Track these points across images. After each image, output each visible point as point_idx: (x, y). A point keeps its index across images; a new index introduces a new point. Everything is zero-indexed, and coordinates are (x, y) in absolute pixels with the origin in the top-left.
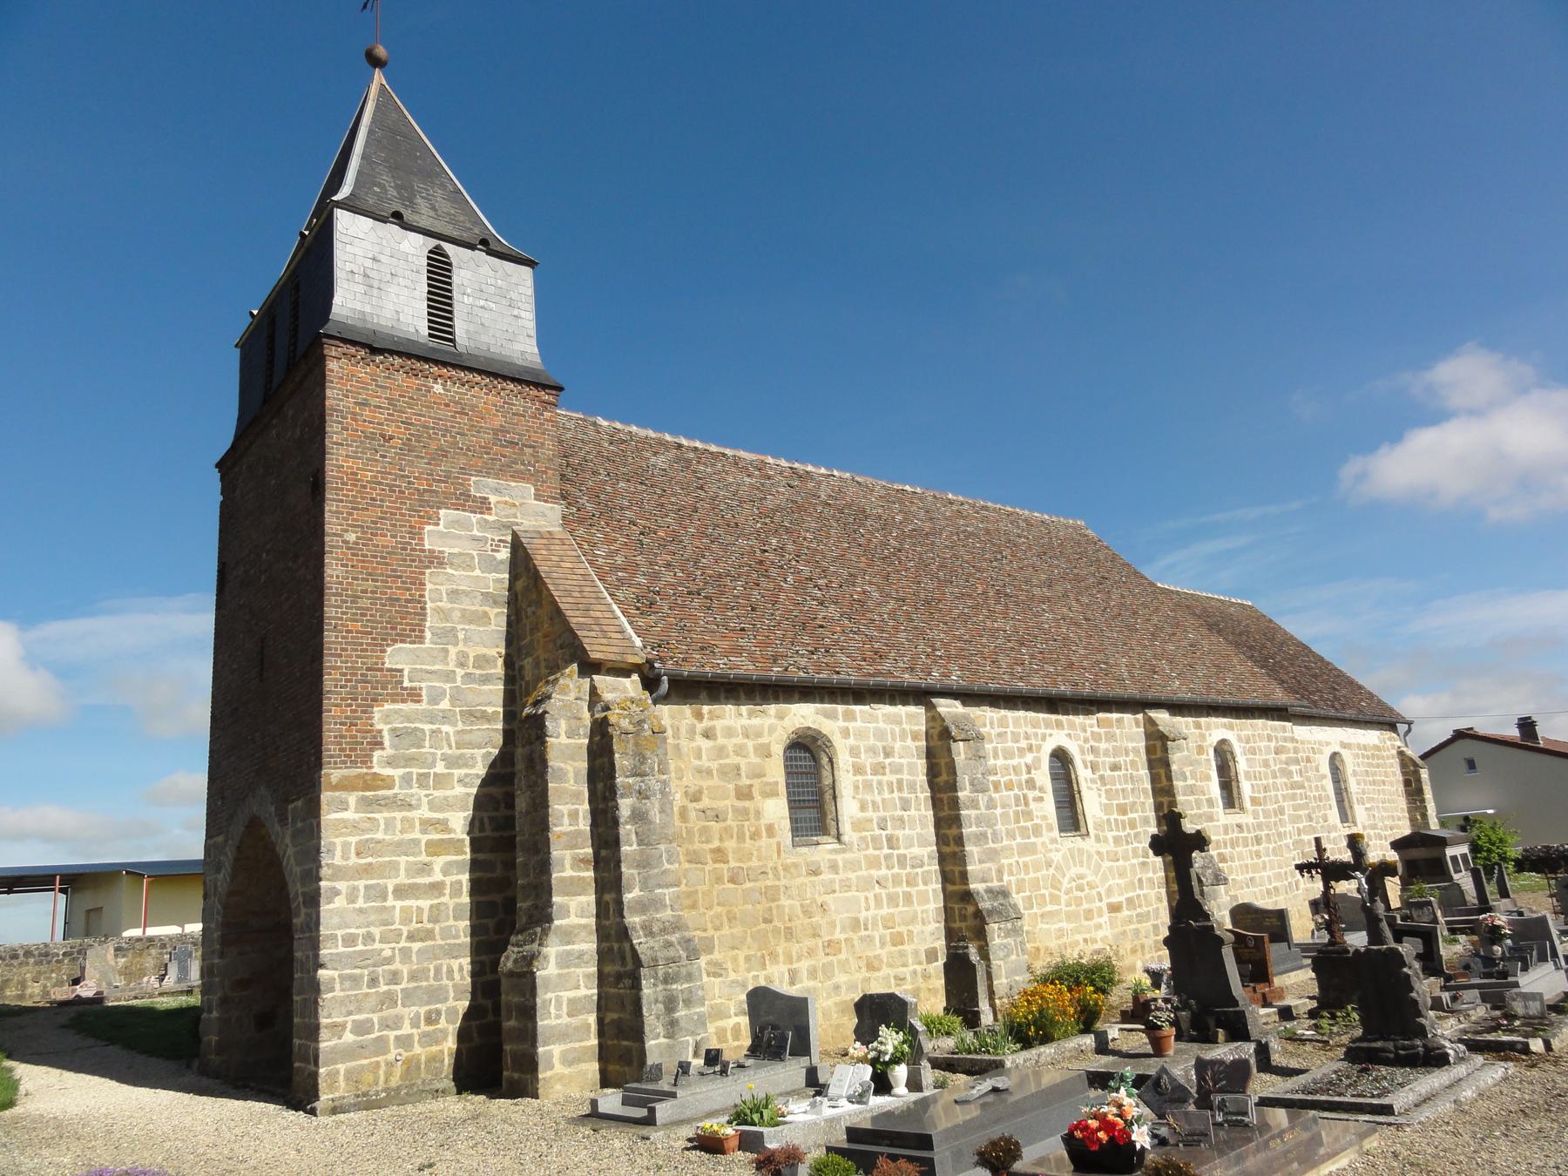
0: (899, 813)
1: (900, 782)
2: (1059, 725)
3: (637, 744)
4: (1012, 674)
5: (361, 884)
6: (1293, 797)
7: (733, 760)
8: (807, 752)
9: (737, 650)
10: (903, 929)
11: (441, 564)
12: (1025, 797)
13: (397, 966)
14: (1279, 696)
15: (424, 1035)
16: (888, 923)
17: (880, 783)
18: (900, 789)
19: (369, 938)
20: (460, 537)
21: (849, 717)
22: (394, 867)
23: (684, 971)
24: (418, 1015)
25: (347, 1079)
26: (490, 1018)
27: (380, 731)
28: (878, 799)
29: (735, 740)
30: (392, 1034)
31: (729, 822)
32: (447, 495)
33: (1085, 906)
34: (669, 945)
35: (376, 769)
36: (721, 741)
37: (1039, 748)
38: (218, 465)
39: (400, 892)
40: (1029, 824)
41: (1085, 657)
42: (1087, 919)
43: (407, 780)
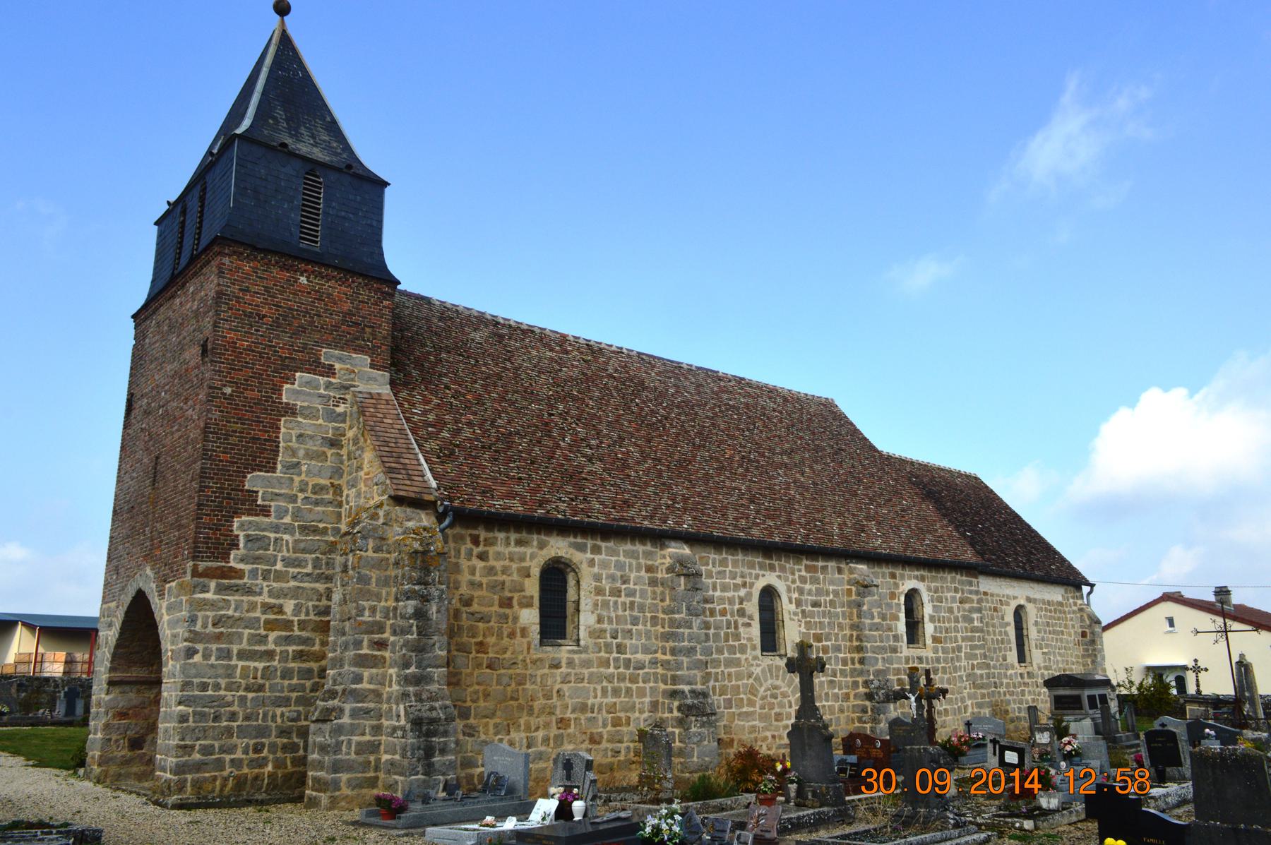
0: (629, 627)
1: (632, 603)
2: (772, 568)
3: (423, 561)
4: (736, 526)
5: (214, 647)
6: (971, 639)
7: (501, 578)
8: (555, 578)
9: (511, 495)
10: (622, 715)
11: (294, 414)
12: (736, 622)
13: (235, 708)
14: (969, 555)
15: (252, 760)
16: (611, 709)
17: (616, 603)
18: (632, 608)
19: (217, 687)
20: (309, 394)
21: (596, 550)
22: (240, 636)
23: (441, 728)
24: (247, 746)
25: (193, 786)
26: (301, 752)
27: (237, 536)
28: (613, 615)
29: (502, 563)
30: (228, 757)
31: (492, 623)
32: (304, 362)
33: (777, 710)
34: (432, 709)
35: (232, 564)
36: (492, 563)
37: (752, 585)
38: (133, 317)
39: (242, 655)
40: (736, 643)
41: (804, 515)
42: (776, 720)
43: (254, 573)
